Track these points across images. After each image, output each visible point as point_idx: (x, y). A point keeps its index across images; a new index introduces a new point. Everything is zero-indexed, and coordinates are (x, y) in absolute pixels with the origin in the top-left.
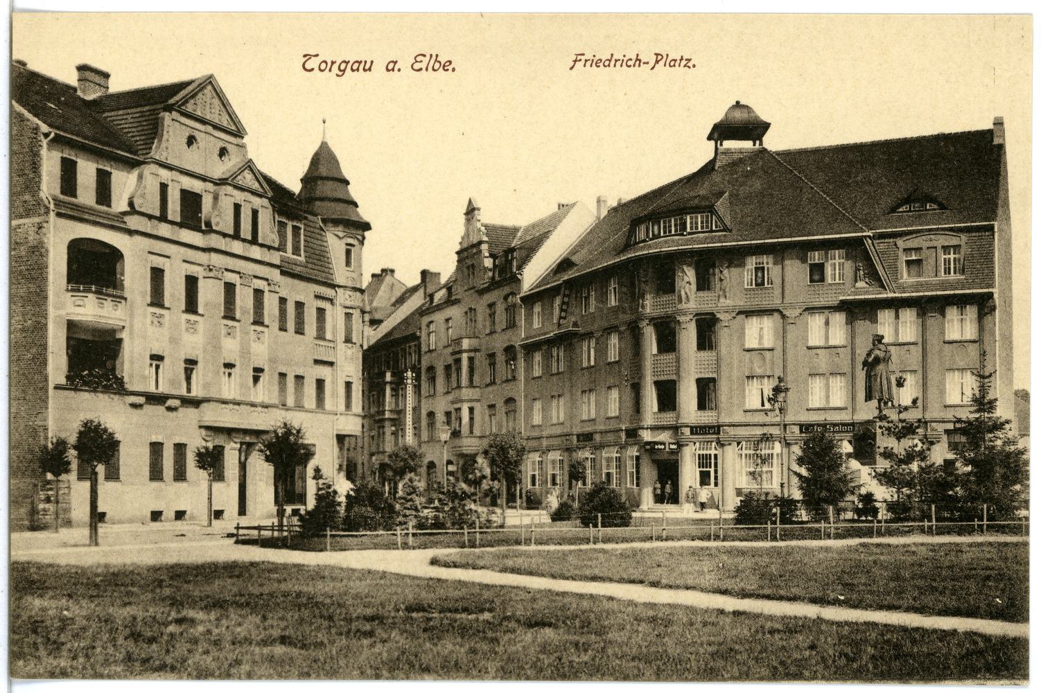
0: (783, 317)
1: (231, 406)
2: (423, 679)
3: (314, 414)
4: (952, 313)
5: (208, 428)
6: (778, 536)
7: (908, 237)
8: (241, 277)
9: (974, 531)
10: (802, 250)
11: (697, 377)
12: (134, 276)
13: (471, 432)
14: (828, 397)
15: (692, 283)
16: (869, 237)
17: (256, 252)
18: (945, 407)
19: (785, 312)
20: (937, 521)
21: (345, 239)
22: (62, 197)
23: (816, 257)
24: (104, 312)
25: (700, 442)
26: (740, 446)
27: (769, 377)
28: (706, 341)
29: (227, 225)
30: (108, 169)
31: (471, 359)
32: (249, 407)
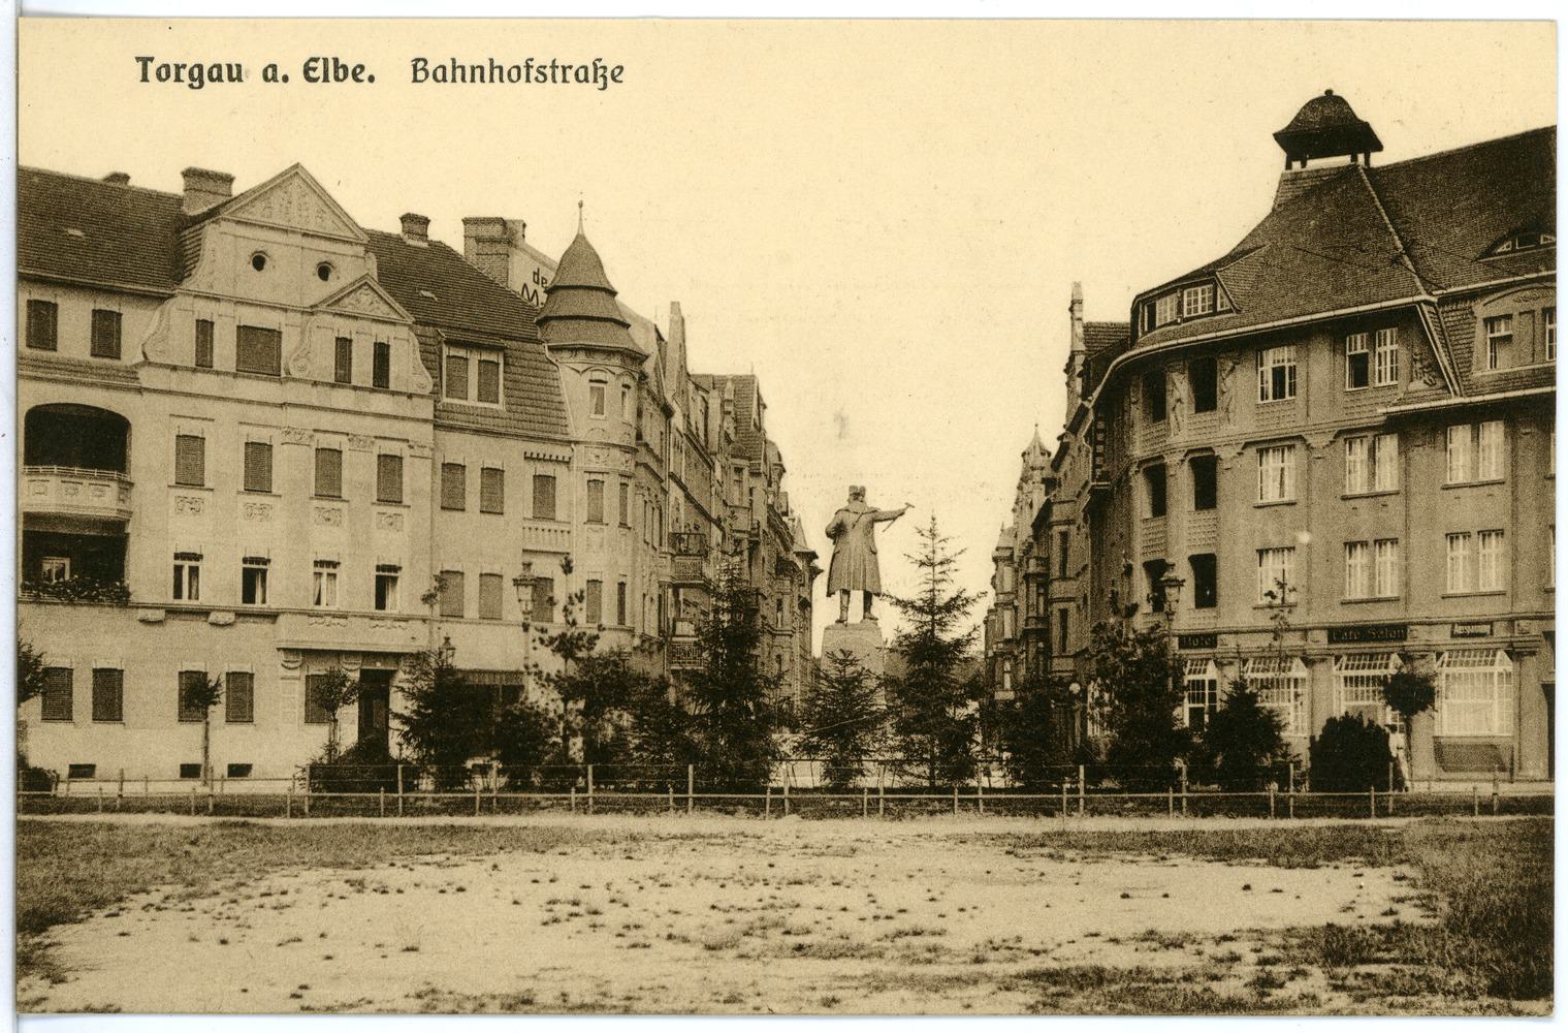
0: (1309, 447)
1: (328, 619)
3: (474, 626)
6: (306, 810)
7: (1508, 291)
9: (667, 809)
10: (1336, 332)
11: (1190, 554)
12: (150, 450)
13: (1064, 649)
14: (1476, 577)
15: (1185, 401)
19: (1310, 440)
20: (694, 791)
21: (589, 372)
22: (28, 352)
24: (75, 501)
25: (1349, 655)
28: (1206, 496)
30: (115, 309)
31: (1064, 536)
32: (367, 620)
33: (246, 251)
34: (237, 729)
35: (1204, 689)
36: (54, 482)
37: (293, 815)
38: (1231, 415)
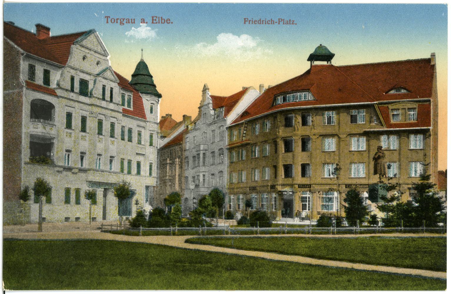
0: (339, 138)
11: (301, 163)
12: (59, 116)
25: (302, 191)
33: (82, 55)
34: (48, 205)
35: (307, 199)
36: (40, 125)
37: (333, 234)
38: (315, 128)
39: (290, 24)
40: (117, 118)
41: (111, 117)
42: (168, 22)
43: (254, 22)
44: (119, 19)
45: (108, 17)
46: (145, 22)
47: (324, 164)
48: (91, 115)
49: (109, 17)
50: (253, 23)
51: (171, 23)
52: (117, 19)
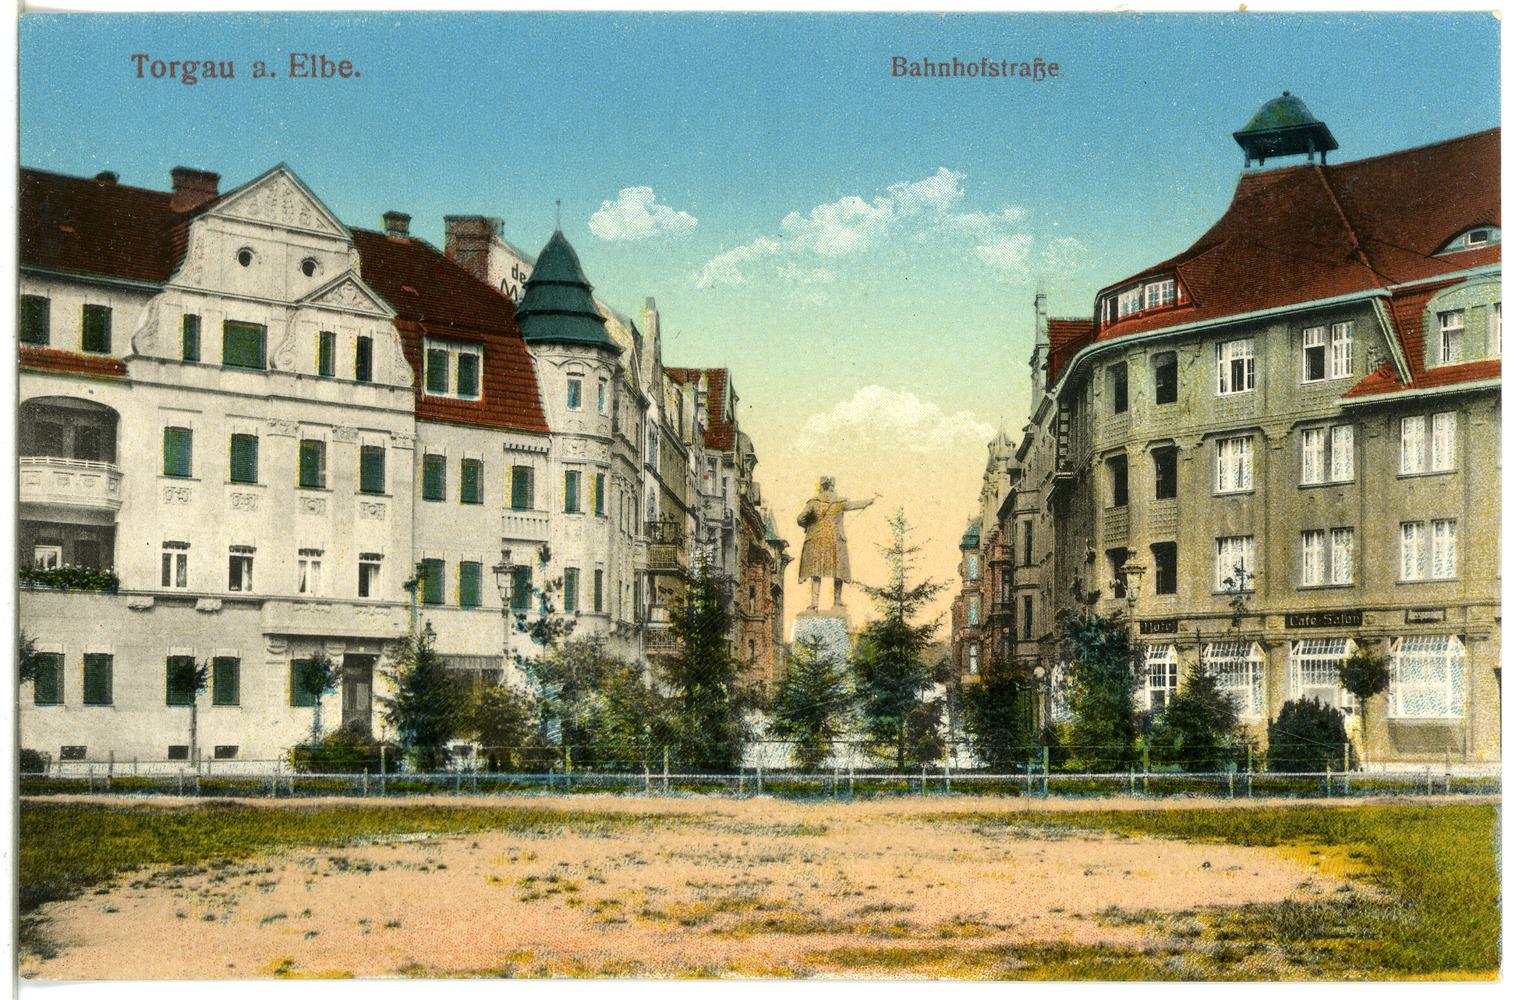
1: (373, 609)
2: (1385, 980)
4: (1413, 429)
5: (273, 636)
8: (334, 432)
12: (139, 438)
16: (1382, 297)
17: (364, 395)
18: (1397, 584)
23: (1315, 338)
26: (1395, 646)
27: (1248, 537)
29: (310, 362)
39: (926, 75)
40: (390, 432)
41: (359, 429)
42: (345, 71)
43: (1050, 68)
44: (178, 63)
45: (140, 57)
46: (268, 72)
47: (1221, 541)
48: (273, 431)
49: (147, 57)
50: (966, 72)
51: (353, 77)
52: (173, 65)
